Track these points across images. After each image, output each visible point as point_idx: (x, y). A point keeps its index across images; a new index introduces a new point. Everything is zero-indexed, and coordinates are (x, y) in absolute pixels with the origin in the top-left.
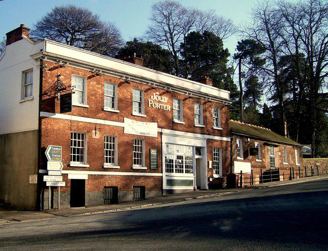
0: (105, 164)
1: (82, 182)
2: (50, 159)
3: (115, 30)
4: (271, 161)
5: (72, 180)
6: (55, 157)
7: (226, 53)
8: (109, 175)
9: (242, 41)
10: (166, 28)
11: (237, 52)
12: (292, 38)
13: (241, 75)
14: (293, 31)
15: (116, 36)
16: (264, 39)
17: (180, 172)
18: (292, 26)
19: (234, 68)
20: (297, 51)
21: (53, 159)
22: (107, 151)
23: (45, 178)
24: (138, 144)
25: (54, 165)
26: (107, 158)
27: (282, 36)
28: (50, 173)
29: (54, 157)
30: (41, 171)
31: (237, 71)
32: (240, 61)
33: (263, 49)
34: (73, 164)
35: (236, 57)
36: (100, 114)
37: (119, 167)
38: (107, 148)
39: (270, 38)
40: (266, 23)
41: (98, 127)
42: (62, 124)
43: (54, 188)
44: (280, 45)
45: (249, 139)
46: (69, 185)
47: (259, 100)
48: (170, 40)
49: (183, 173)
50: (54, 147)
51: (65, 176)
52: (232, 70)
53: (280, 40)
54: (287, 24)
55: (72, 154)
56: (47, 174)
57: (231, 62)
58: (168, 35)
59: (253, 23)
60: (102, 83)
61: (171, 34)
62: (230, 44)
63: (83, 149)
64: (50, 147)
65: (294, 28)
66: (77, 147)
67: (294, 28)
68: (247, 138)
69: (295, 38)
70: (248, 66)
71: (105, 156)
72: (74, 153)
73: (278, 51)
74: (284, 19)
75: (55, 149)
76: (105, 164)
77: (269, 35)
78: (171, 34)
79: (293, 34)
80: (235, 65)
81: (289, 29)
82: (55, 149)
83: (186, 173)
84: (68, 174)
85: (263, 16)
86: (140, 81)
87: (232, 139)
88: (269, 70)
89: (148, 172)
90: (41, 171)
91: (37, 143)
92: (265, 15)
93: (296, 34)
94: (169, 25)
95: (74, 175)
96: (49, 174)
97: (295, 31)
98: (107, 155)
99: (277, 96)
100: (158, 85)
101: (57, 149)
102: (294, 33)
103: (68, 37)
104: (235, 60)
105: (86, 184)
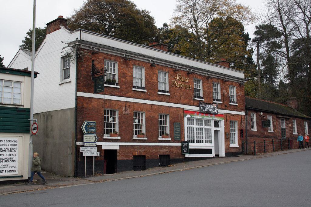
0: (135, 136)
1: (115, 151)
2: (86, 132)
3: (149, 17)
4: (282, 132)
5: (106, 151)
6: (90, 131)
7: (246, 37)
8: (138, 146)
9: (260, 25)
10: (191, 16)
11: (255, 36)
12: (303, 23)
13: (259, 56)
14: (305, 17)
15: (148, 21)
16: (277, 24)
17: (201, 143)
18: (304, 12)
19: (254, 49)
20: (308, 35)
21: (89, 132)
22: (161, 126)
23: (82, 149)
24: (164, 119)
25: (90, 138)
26: (136, 131)
27: (294, 21)
28: (86, 145)
29: (89, 131)
30: (78, 143)
31: (255, 52)
32: (258, 44)
33: (279, 34)
34: (106, 136)
35: (254, 41)
36: (129, 94)
37: (146, 139)
38: (161, 124)
39: (282, 24)
40: (279, 10)
41: (128, 105)
42: (96, 103)
43: (90, 158)
44: (292, 30)
45: (262, 114)
46: (103, 154)
47: (276, 79)
48: (195, 26)
49: (203, 143)
50: (89, 122)
51: (99, 147)
52: (252, 51)
53: (291, 25)
54: (299, 11)
55: (106, 128)
56: (83, 146)
57: (251, 46)
58: (193, 23)
59: (267, 10)
60: (131, 66)
61: (196, 21)
62: (250, 29)
63: (142, 125)
64: (86, 123)
65: (305, 14)
66: (106, 122)
67: (305, 14)
68: (261, 112)
69: (306, 23)
70: (265, 48)
71: (134, 130)
72: (107, 127)
73: (290, 35)
74: (296, 7)
75: (90, 124)
76: (135, 136)
77: (282, 21)
78: (196, 21)
79: (305, 20)
80: (254, 47)
81: (301, 15)
82: (90, 124)
83: (197, 142)
84: (102, 145)
85: (277, 5)
86: (165, 64)
87: (246, 114)
88: (282, 52)
89: (172, 143)
90: (78, 143)
91: (174, 62)
92: (278, 3)
93: (307, 19)
94: (194, 14)
95: (106, 146)
96: (85, 146)
97: (306, 17)
98: (136, 128)
99: (291, 75)
100: (180, 68)
101: (92, 124)
102: (305, 19)
103: (106, 24)
104: (253, 43)
105: (118, 154)
